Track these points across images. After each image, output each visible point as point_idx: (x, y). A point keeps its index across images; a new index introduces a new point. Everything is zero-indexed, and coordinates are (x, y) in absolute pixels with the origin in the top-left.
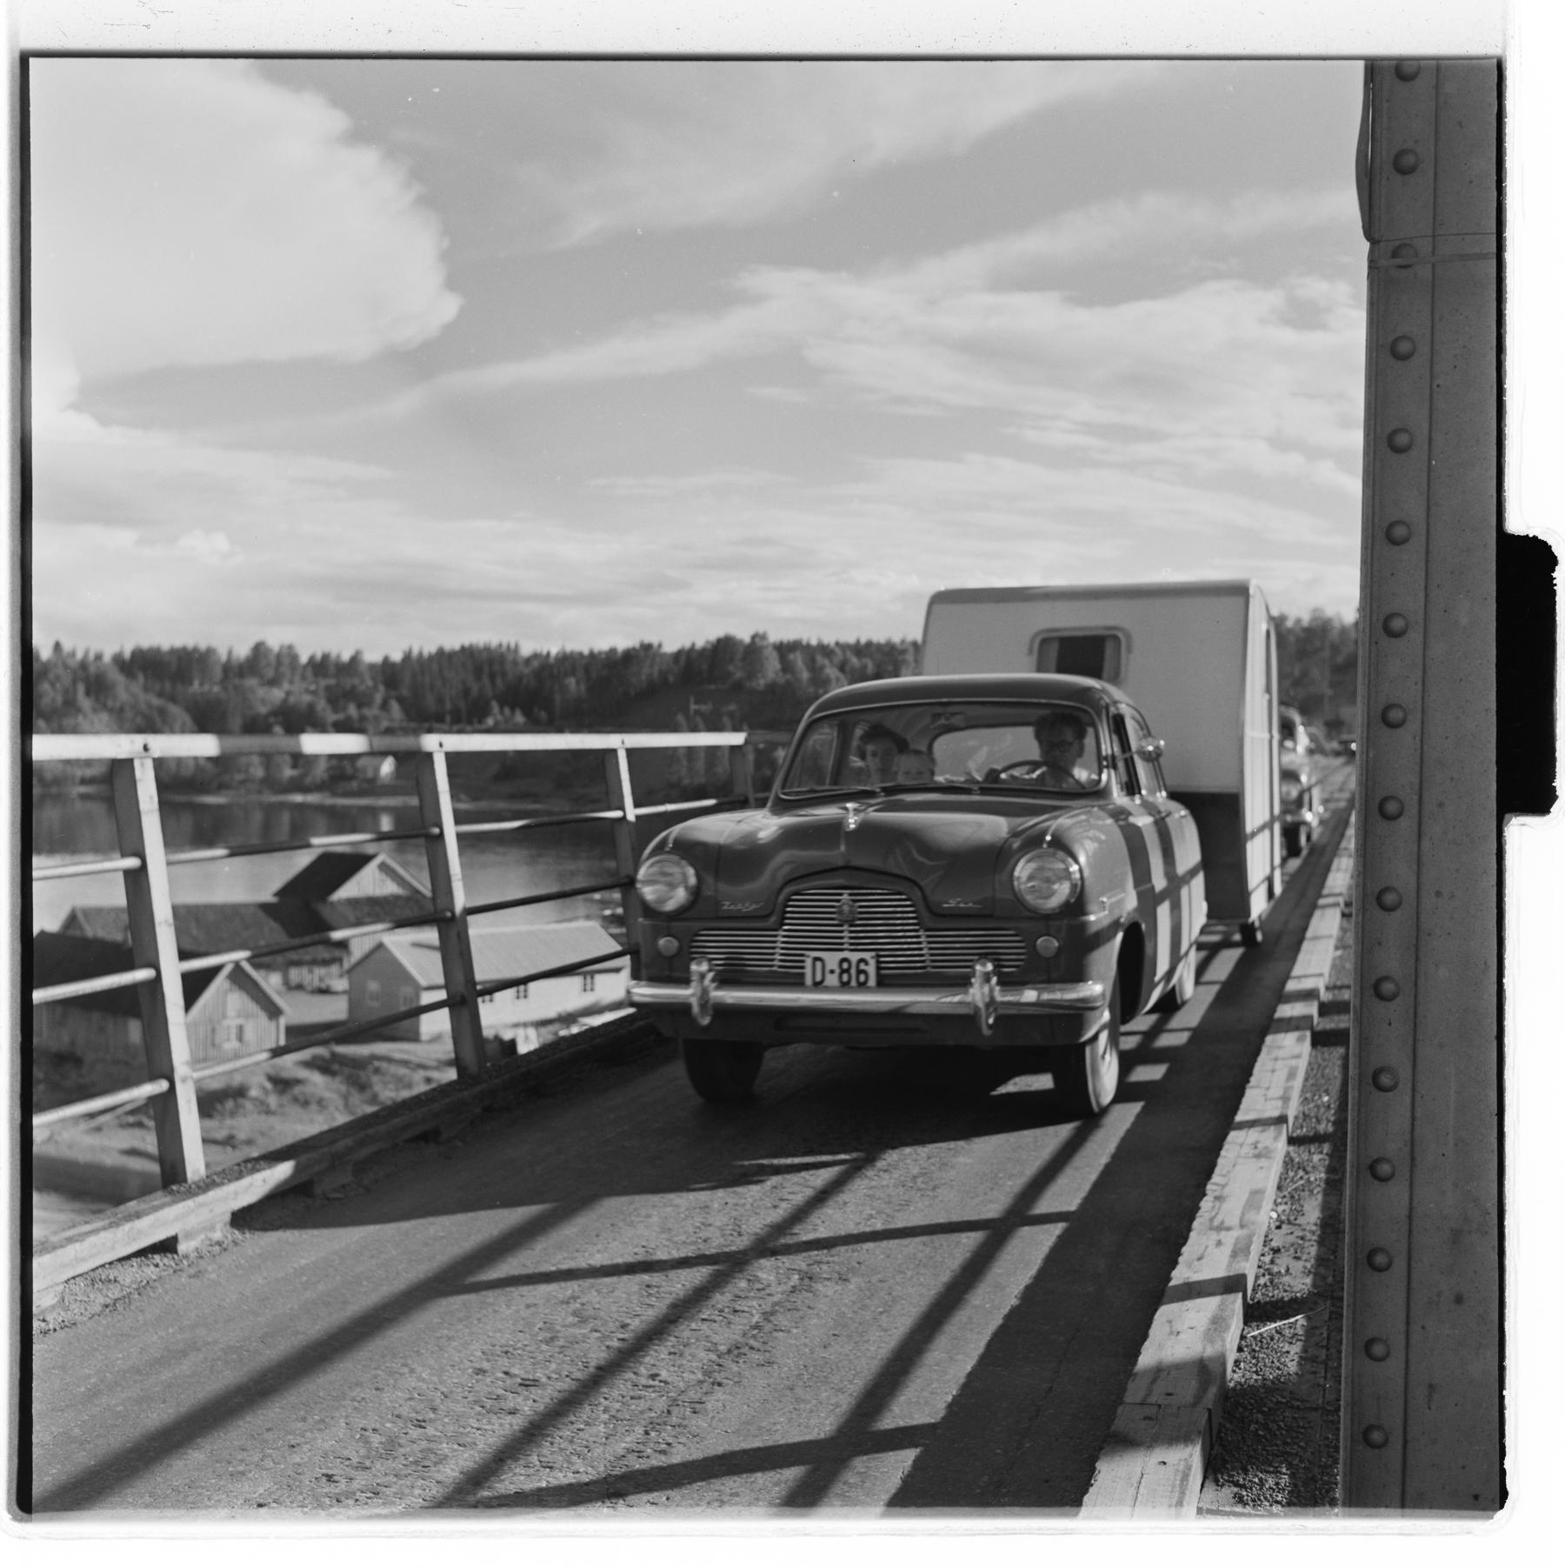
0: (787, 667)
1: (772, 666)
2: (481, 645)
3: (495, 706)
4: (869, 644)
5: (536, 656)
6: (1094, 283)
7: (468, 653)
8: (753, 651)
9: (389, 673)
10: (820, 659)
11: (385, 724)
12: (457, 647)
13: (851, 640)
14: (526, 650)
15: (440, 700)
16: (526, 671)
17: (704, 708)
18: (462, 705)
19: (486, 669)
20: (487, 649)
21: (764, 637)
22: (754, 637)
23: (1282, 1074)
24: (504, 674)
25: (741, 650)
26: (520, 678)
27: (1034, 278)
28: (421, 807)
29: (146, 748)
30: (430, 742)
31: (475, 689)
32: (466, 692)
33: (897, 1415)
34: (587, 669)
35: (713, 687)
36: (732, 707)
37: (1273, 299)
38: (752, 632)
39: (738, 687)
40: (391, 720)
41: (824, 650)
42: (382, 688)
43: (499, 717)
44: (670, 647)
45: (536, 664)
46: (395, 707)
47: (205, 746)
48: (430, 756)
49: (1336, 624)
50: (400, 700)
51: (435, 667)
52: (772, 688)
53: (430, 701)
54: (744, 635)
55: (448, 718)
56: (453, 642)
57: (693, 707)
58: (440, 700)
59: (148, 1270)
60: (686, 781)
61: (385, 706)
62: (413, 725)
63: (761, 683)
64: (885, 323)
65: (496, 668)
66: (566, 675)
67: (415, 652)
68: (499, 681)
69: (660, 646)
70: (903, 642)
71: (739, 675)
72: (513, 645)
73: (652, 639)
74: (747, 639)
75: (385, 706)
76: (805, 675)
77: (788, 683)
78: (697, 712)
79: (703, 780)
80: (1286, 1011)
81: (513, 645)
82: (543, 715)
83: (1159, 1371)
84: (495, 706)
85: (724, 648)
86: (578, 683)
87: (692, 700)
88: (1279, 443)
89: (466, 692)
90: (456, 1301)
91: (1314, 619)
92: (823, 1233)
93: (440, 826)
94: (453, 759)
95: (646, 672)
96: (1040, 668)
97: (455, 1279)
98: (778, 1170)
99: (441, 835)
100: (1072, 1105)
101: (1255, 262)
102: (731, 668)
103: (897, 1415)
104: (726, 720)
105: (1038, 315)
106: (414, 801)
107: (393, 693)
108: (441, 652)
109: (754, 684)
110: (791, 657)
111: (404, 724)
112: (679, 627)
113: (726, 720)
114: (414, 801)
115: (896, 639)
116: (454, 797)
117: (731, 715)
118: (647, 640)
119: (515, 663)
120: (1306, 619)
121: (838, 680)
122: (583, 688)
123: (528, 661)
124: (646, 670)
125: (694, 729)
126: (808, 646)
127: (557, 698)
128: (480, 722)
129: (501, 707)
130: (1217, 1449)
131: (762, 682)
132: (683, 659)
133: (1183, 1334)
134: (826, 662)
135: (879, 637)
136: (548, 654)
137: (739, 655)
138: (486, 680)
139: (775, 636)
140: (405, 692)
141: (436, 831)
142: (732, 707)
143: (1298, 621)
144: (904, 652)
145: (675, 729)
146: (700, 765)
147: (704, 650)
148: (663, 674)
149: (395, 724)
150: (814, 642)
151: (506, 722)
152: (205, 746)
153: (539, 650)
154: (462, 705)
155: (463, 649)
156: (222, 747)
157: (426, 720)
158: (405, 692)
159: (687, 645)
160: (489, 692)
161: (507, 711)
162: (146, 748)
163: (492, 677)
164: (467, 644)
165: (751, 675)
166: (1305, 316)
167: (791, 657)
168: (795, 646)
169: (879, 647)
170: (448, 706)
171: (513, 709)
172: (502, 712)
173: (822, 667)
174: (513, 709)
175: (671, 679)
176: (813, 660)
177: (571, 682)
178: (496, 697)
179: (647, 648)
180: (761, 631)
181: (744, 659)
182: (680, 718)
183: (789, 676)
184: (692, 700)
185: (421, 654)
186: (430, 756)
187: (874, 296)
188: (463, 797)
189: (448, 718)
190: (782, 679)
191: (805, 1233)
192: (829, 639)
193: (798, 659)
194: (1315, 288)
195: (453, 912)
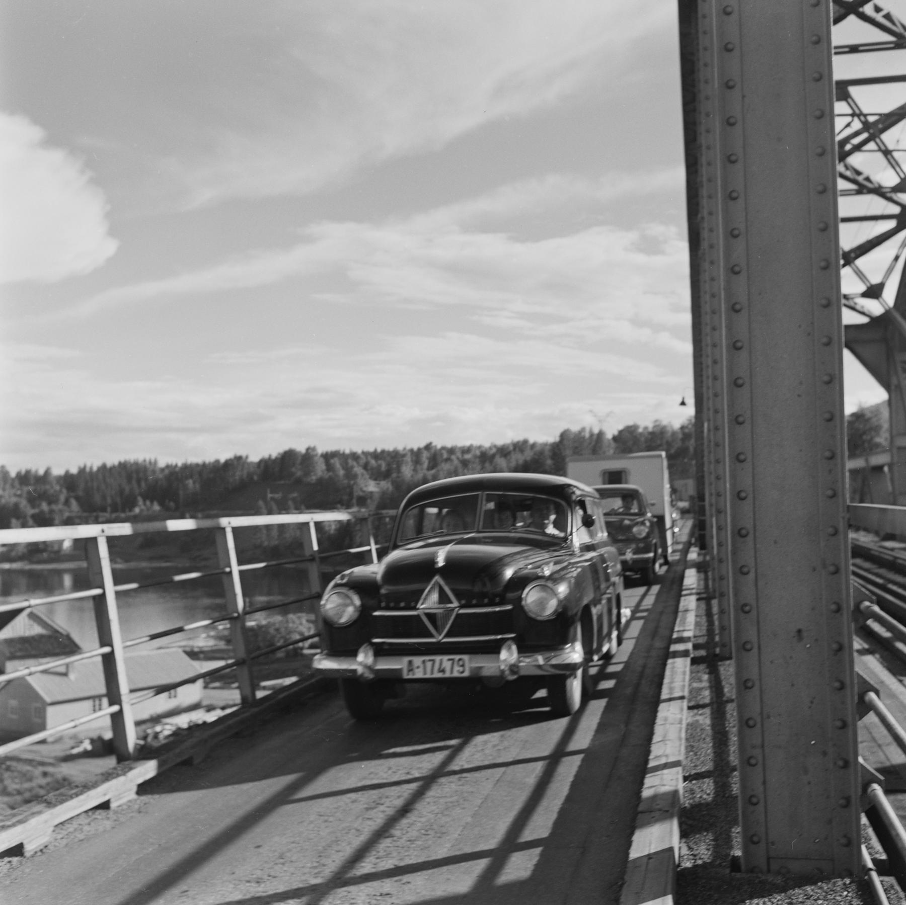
0: (330, 467)
1: (320, 468)
2: (132, 461)
3: (140, 501)
4: (383, 452)
5: (168, 466)
6: (523, 228)
7: (123, 466)
8: (308, 457)
9: (69, 481)
10: (351, 462)
11: (67, 514)
12: (116, 463)
13: (372, 450)
14: (162, 464)
15: (104, 497)
16: (161, 476)
17: (278, 496)
18: (118, 500)
19: (134, 476)
20: (136, 463)
21: (314, 449)
22: (308, 449)
23: (679, 675)
24: (146, 480)
25: (300, 458)
26: (156, 481)
27: (485, 225)
28: (88, 568)
29: (103, 531)
30: (225, 522)
31: (127, 489)
32: (121, 492)
33: (528, 835)
34: (200, 474)
35: (282, 482)
36: (295, 495)
37: (632, 236)
38: (306, 446)
39: (299, 481)
40: (71, 512)
41: (354, 456)
42: (64, 491)
43: (143, 507)
44: (254, 458)
45: (167, 472)
46: (74, 504)
47: (340, 516)
48: (224, 529)
49: (669, 429)
50: (77, 499)
51: (100, 476)
52: (320, 481)
53: (97, 499)
54: (301, 448)
55: (109, 509)
56: (113, 459)
57: (270, 495)
58: (104, 497)
59: (100, 814)
60: (266, 544)
61: (67, 503)
62: (85, 514)
63: (313, 478)
64: (400, 253)
65: (141, 475)
66: (187, 478)
67: (88, 469)
68: (143, 484)
69: (247, 457)
70: (405, 449)
71: (299, 474)
72: (153, 461)
73: (242, 452)
74: (303, 451)
75: (67, 503)
76: (342, 472)
77: (330, 477)
78: (272, 499)
79: (276, 543)
80: (674, 648)
81: (153, 461)
82: (172, 504)
83: (654, 797)
84: (140, 501)
85: (288, 457)
86: (194, 483)
87: (268, 491)
88: (637, 322)
89: (121, 492)
90: (289, 807)
91: (654, 427)
92: (456, 768)
93: (230, 566)
94: (235, 530)
95: (238, 475)
96: (604, 484)
97: (283, 798)
98: (395, 755)
99: (230, 573)
100: (558, 707)
101: (622, 214)
102: (293, 469)
103: (528, 835)
104: (290, 503)
105: (492, 247)
106: (84, 564)
107: (72, 494)
108: (104, 467)
109: (309, 479)
110: (332, 461)
111: (79, 514)
112: (260, 446)
113: (290, 503)
114: (84, 564)
115: (400, 448)
116: (112, 560)
117: (294, 500)
118: (238, 454)
119: (154, 472)
120: (650, 426)
121: (363, 475)
122: (198, 486)
123: (162, 470)
124: (238, 474)
125: (270, 512)
126: (344, 454)
127: (181, 492)
128: (130, 510)
129: (144, 501)
130: (684, 827)
131: (314, 478)
132: (262, 465)
133: (660, 783)
134: (355, 464)
135: (390, 447)
136: (176, 466)
137: (298, 462)
138: (134, 482)
139: (321, 450)
140: (80, 493)
141: (228, 570)
142: (295, 495)
143: (646, 428)
144: (404, 456)
145: (257, 512)
146: (275, 533)
147: (276, 459)
148: (250, 475)
149: (74, 514)
150: (347, 451)
151: (148, 510)
152: (340, 516)
153: (170, 463)
154: (118, 500)
155: (120, 463)
156: (134, 530)
157: (95, 511)
158: (80, 493)
159: (266, 456)
160: (137, 491)
161: (148, 503)
162: (103, 531)
163: (139, 481)
164: (122, 460)
165: (307, 473)
166: (651, 246)
167: (332, 461)
168: (335, 454)
169: (389, 453)
170: (109, 501)
171: (152, 502)
172: (145, 504)
173: (352, 467)
174: (152, 502)
175: (255, 478)
176: (347, 463)
177: (190, 482)
178: (141, 495)
179: (238, 458)
180: (312, 446)
181: (301, 464)
182: (261, 503)
183: (331, 474)
184: (268, 491)
185: (91, 468)
186: (224, 529)
187: (392, 237)
188: (119, 560)
189: (109, 509)
190: (327, 475)
191: (414, 786)
192: (358, 450)
193: (336, 462)
194: (656, 229)
195: (237, 611)
